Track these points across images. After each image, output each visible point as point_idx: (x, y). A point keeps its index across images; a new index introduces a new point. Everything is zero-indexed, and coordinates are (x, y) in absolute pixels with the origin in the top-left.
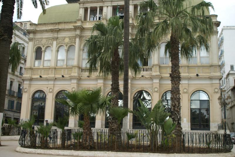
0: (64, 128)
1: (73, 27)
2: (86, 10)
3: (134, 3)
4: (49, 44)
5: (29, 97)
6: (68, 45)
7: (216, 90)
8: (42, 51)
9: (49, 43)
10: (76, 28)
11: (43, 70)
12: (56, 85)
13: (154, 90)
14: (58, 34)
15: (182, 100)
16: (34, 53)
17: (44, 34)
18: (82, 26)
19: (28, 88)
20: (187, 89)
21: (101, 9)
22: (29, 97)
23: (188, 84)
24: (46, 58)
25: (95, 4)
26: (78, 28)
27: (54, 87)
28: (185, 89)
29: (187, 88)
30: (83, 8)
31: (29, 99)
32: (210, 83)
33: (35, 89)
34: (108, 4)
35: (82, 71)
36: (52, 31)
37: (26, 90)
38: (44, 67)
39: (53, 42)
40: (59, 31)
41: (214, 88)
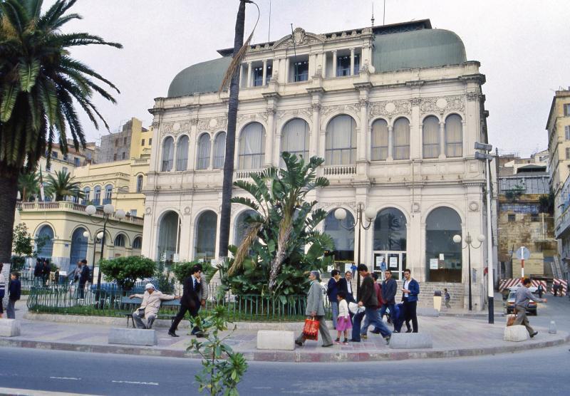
0: (6, 263)
1: (306, 92)
2: (329, 57)
3: (325, 50)
7: (474, 206)
9: (456, 107)
10: (360, 87)
12: (159, 203)
15: (465, 225)
18: (278, 93)
21: (270, 63)
23: (422, 195)
26: (316, 92)
29: (190, 207)
36: (409, 85)
41: (470, 201)
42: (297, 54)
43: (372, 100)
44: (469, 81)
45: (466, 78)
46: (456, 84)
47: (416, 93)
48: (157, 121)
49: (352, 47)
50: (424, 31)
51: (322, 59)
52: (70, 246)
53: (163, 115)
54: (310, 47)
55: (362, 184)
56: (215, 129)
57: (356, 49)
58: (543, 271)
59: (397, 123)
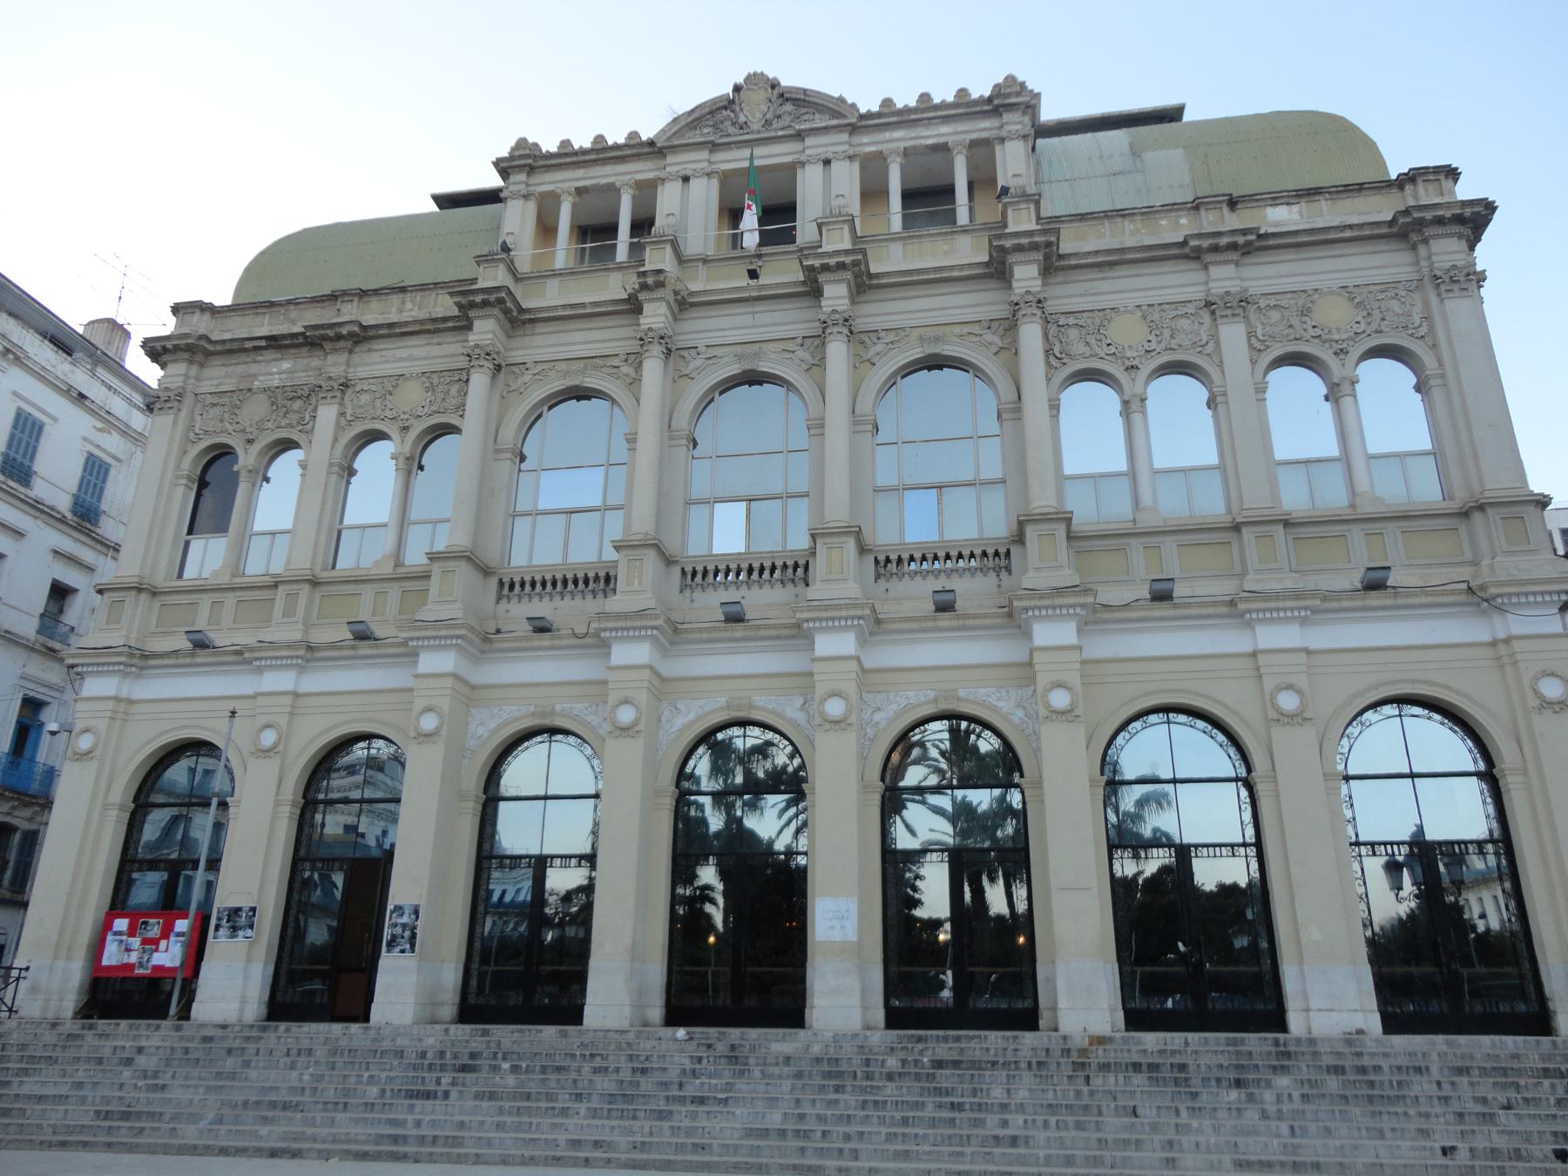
4: (290, 426)
5: (108, 789)
6: (418, 427)
8: (238, 473)
11: (230, 599)
13: (1047, 705)
14: (356, 359)
16: (180, 491)
17: (538, 340)
19: (102, 725)
20: (1299, 692)
22: (108, 789)
24: (261, 523)
25: (608, 169)
27: (292, 714)
28: (1290, 687)
29: (1302, 681)
30: (851, 158)
31: (106, 806)
32: (1487, 638)
33: (160, 735)
34: (694, 166)
35: (506, 591)
37: (85, 743)
38: (400, 570)
39: (315, 410)
40: (363, 336)
42: (757, 163)
43: (518, 356)
44: (1440, 230)
45: (1205, 243)
46: (1383, 246)
47: (1225, 277)
48: (176, 383)
51: (847, 179)
52: (390, 907)
53: (202, 365)
54: (799, 136)
57: (974, 144)
58: (627, 1011)
59: (723, 401)
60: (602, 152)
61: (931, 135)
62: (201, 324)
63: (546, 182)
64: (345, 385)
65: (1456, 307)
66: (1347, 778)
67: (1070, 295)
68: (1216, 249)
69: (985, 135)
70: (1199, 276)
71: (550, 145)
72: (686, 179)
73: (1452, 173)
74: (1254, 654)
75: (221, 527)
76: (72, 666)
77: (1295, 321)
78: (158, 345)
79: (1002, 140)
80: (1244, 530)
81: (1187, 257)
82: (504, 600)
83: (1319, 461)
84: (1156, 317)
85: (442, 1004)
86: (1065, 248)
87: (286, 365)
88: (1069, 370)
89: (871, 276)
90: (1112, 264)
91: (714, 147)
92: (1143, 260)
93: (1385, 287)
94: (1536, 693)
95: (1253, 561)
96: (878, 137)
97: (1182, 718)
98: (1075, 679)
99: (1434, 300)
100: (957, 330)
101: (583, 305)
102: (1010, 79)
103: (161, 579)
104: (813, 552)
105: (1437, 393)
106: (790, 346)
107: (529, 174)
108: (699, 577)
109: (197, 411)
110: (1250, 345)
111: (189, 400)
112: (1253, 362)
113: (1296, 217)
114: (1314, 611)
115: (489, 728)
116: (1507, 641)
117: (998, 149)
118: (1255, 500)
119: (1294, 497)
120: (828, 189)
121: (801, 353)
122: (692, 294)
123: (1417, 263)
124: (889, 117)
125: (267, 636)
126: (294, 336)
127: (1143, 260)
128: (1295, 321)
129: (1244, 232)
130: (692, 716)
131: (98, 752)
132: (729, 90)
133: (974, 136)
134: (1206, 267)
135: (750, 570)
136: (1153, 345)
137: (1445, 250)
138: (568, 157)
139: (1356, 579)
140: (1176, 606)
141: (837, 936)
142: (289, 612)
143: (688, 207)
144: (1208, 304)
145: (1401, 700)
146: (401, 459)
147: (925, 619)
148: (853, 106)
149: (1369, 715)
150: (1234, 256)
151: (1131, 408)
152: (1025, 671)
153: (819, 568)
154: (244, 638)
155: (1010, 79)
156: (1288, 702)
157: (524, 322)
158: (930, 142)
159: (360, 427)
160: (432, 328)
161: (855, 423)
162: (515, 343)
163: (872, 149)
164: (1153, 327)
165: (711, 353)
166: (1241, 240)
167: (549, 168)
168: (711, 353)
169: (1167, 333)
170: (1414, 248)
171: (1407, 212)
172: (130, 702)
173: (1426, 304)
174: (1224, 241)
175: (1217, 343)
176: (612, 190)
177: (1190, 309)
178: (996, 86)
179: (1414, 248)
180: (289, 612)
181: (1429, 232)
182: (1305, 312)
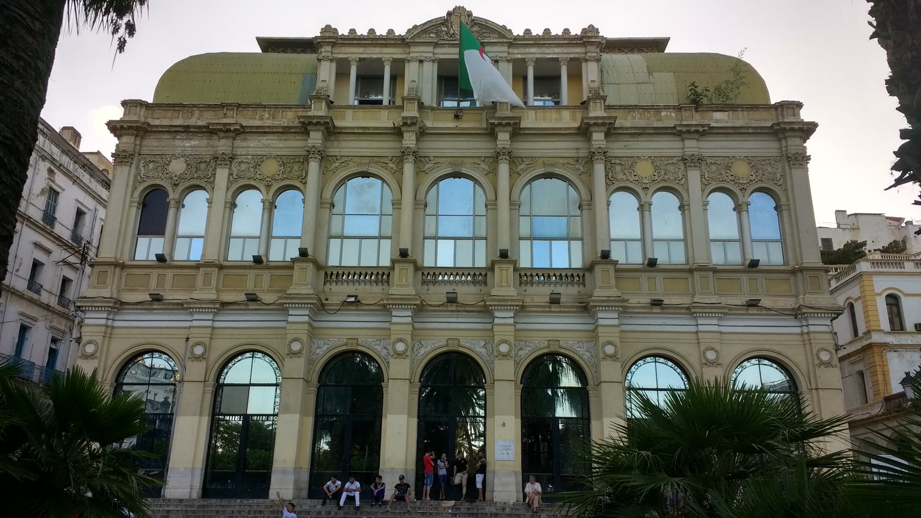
17: (343, 144)
19: (99, 339)
24: (182, 229)
25: (377, 50)
28: (712, 349)
40: (242, 131)
43: (333, 151)
45: (684, 129)
47: (692, 146)
48: (130, 149)
49: (354, 56)
50: (655, 55)
53: (142, 138)
55: (401, 303)
56: (181, 177)
57: (395, 61)
60: (372, 40)
61: (551, 53)
62: (140, 116)
63: (343, 53)
64: (232, 158)
65: (796, 172)
66: (276, 385)
67: (618, 149)
68: (689, 132)
69: (577, 56)
70: (680, 145)
71: (343, 31)
72: (421, 62)
73: (799, 105)
74: (697, 333)
75: (159, 231)
76: (79, 307)
77: (723, 172)
78: (118, 126)
79: (587, 60)
80: (695, 273)
81: (674, 134)
82: (328, 284)
83: (729, 241)
84: (658, 163)
85: (301, 489)
86: (617, 124)
87: (193, 143)
88: (615, 186)
89: (521, 129)
90: (639, 134)
91: (436, 45)
92: (653, 134)
93: (765, 159)
94: (818, 358)
95: (698, 288)
96: (522, 50)
97: (662, 360)
98: (617, 341)
99: (787, 168)
100: (561, 161)
101: (369, 128)
102: (591, 26)
103: (126, 259)
104: (392, 268)
105: (785, 213)
106: (477, 161)
107: (332, 47)
108: (334, 277)
109: (141, 165)
110: (702, 182)
111: (136, 157)
112: (703, 191)
113: (726, 118)
114: (725, 314)
115: (222, 346)
116: (808, 333)
117: (584, 65)
118: (701, 260)
119: (717, 257)
120: (488, 77)
121: (483, 166)
122: (428, 128)
123: (781, 148)
124: (528, 40)
125: (196, 295)
126: (200, 127)
127: (653, 134)
128: (723, 172)
129: (703, 126)
130: (428, 349)
131: (98, 354)
132: (445, 14)
133: (572, 56)
134: (683, 140)
135: (360, 274)
136: (656, 177)
137: (792, 143)
138: (353, 39)
139: (646, 300)
140: (560, 307)
141: (505, 457)
142: (207, 283)
143: (422, 78)
144: (684, 159)
145: (655, 356)
146: (267, 203)
147: (545, 307)
148: (510, 31)
149: (745, 363)
150: (697, 136)
151: (644, 208)
152: (593, 335)
153: (396, 275)
154: (180, 296)
155: (591, 26)
156: (711, 355)
157: (335, 133)
158: (550, 56)
159: (242, 182)
160: (286, 131)
161: (416, 204)
162: (329, 144)
163: (519, 56)
164: (657, 168)
165: (437, 160)
166: (701, 129)
167: (344, 45)
168: (437, 160)
169: (663, 172)
170: (780, 140)
171: (778, 124)
172: (113, 327)
173: (784, 169)
174: (693, 129)
175: (687, 179)
176: (380, 62)
177: (675, 161)
178: (463, 31)
179: (780, 140)
180: (207, 283)
181: (787, 134)
182: (728, 168)
